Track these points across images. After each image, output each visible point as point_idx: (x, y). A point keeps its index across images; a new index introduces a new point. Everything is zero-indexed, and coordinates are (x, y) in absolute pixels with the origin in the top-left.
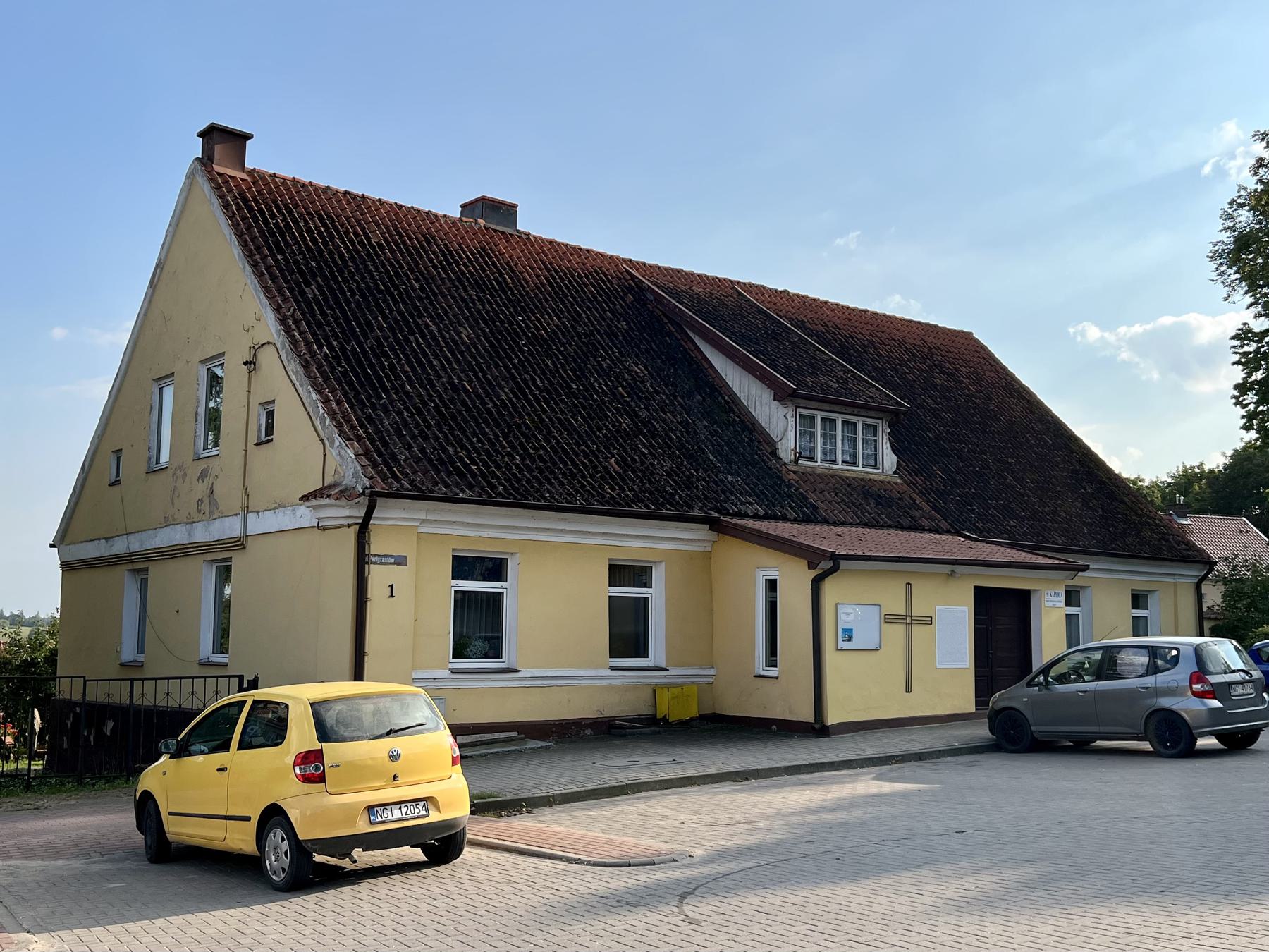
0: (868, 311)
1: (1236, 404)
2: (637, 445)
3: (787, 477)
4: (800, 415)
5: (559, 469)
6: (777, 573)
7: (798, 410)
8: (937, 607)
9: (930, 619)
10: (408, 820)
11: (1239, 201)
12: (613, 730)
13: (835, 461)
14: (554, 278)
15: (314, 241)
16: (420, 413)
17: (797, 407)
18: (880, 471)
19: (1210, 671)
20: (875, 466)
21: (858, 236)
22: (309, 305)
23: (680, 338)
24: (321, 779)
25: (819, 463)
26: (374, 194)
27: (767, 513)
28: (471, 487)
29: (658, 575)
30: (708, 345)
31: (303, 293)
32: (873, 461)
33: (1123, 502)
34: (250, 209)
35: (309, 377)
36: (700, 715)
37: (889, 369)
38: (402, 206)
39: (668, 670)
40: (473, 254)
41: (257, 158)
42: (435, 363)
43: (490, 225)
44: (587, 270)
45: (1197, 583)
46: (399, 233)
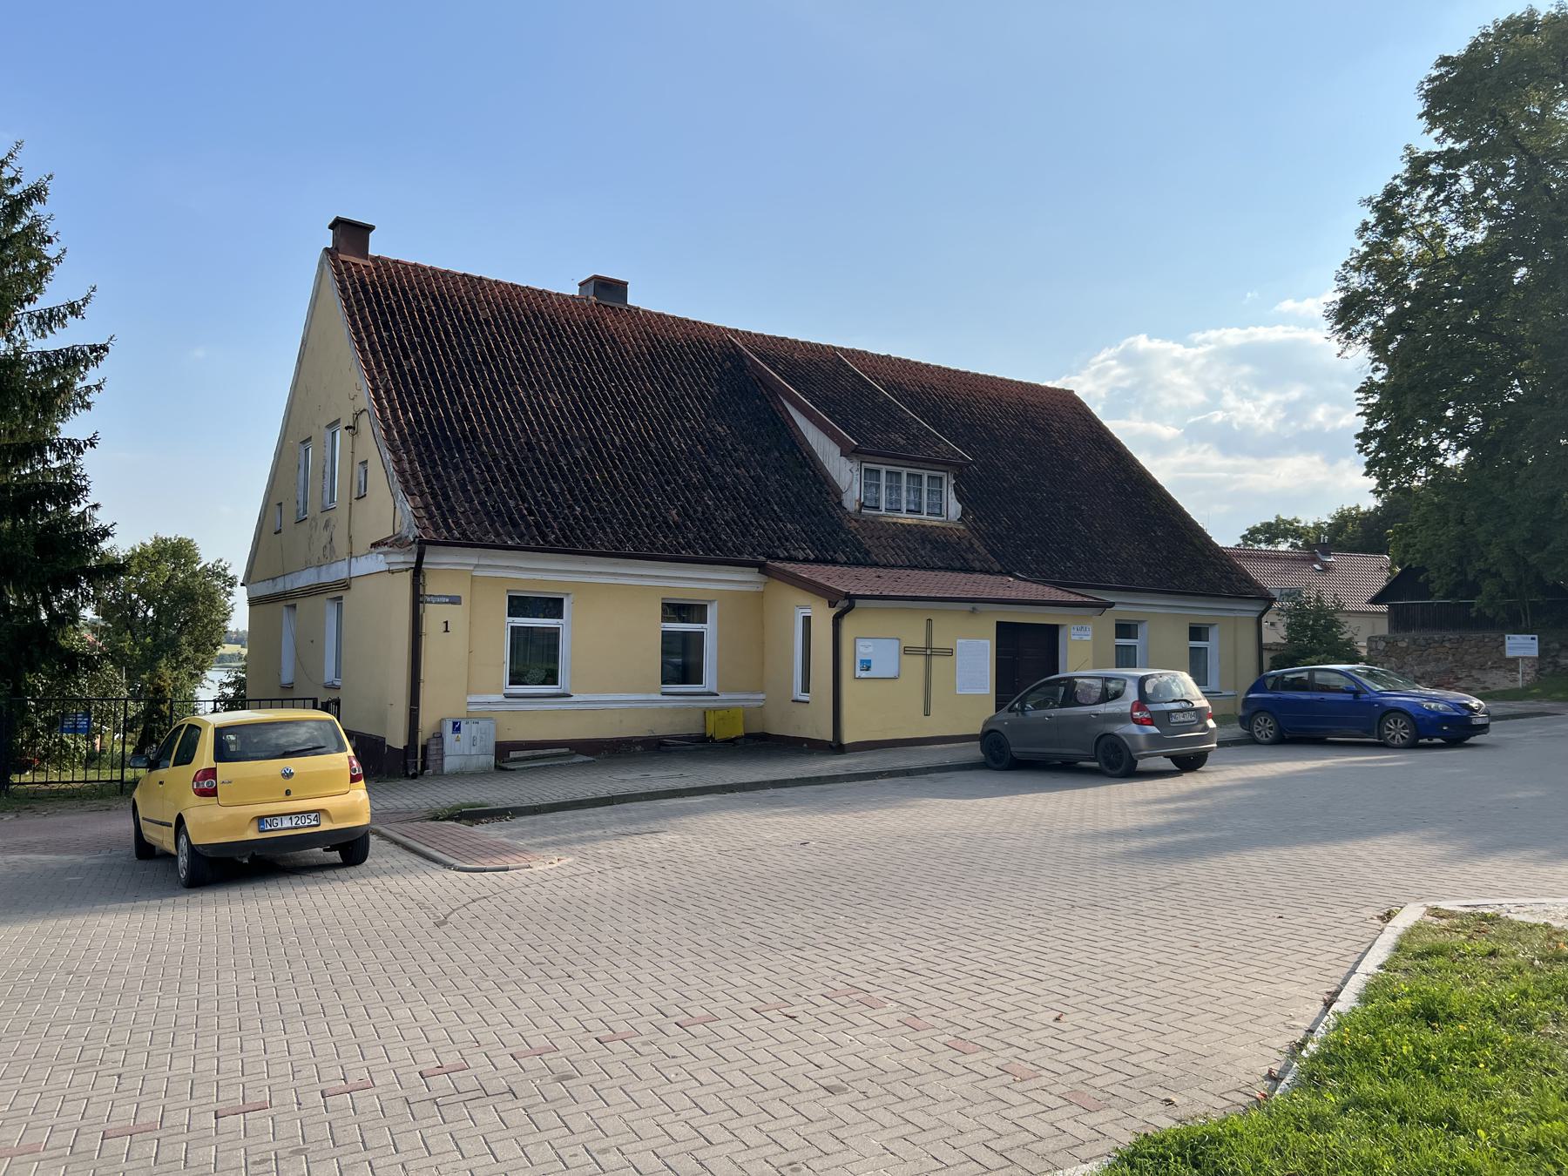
1: (1359, 452)
2: (702, 498)
5: (618, 519)
6: (809, 611)
11: (1352, 263)
14: (655, 348)
15: (423, 319)
16: (489, 469)
17: (861, 462)
20: (940, 515)
24: (212, 792)
25: (883, 512)
26: (491, 275)
27: (817, 557)
28: (521, 536)
29: (712, 612)
33: (1192, 544)
34: (366, 292)
38: (517, 286)
41: (377, 246)
46: (507, 310)
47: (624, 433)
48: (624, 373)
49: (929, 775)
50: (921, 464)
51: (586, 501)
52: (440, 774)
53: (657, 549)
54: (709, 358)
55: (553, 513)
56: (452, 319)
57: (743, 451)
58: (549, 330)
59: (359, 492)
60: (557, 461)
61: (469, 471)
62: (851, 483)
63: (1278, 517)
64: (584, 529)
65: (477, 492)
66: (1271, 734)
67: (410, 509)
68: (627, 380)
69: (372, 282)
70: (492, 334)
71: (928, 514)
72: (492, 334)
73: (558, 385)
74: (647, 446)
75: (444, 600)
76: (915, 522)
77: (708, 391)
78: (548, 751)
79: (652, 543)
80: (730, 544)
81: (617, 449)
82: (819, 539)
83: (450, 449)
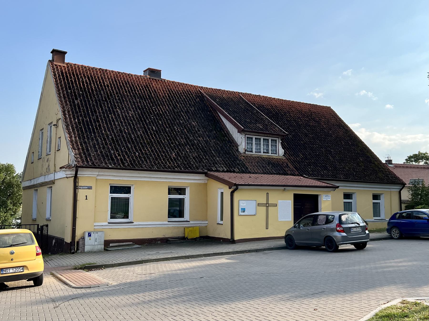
0: (290, 101)
2: (185, 149)
3: (240, 158)
4: (247, 137)
5: (152, 157)
6: (223, 190)
7: (246, 136)
9: (276, 205)
10: (15, 273)
12: (168, 242)
13: (260, 152)
15: (84, 85)
16: (105, 139)
17: (245, 135)
18: (278, 155)
19: (343, 223)
20: (276, 154)
21: (352, 71)
22: (75, 106)
23: (213, 112)
25: (254, 153)
27: (227, 170)
28: (115, 164)
29: (187, 191)
30: (222, 115)
31: (74, 102)
32: (275, 151)
33: (374, 163)
34: (63, 76)
35: (67, 129)
36: (200, 236)
37: (293, 120)
38: (120, 72)
39: (190, 222)
40: (142, 87)
41: (68, 59)
42: (116, 123)
43: (151, 77)
44: (184, 91)
45: (399, 191)
46: (116, 81)
47: (157, 126)
48: (158, 103)
49: (265, 252)
50: (268, 135)
51: (141, 150)
52: (83, 252)
53: (166, 168)
54: (191, 98)
55: (128, 155)
56: (94, 85)
57: (202, 131)
58: (131, 88)
59: (58, 148)
60: (131, 136)
61: (97, 140)
62: (242, 142)
63: (419, 152)
64: (139, 161)
65: (100, 148)
66: (398, 235)
67: (73, 155)
68: (159, 106)
69: (66, 72)
70: (109, 90)
71: (271, 153)
72: (109, 90)
73: (133, 108)
74: (165, 130)
75: (85, 188)
76: (267, 157)
77: (190, 109)
78: (124, 243)
79: (165, 166)
80: (194, 166)
81: (154, 131)
82: (228, 163)
83: (90, 133)
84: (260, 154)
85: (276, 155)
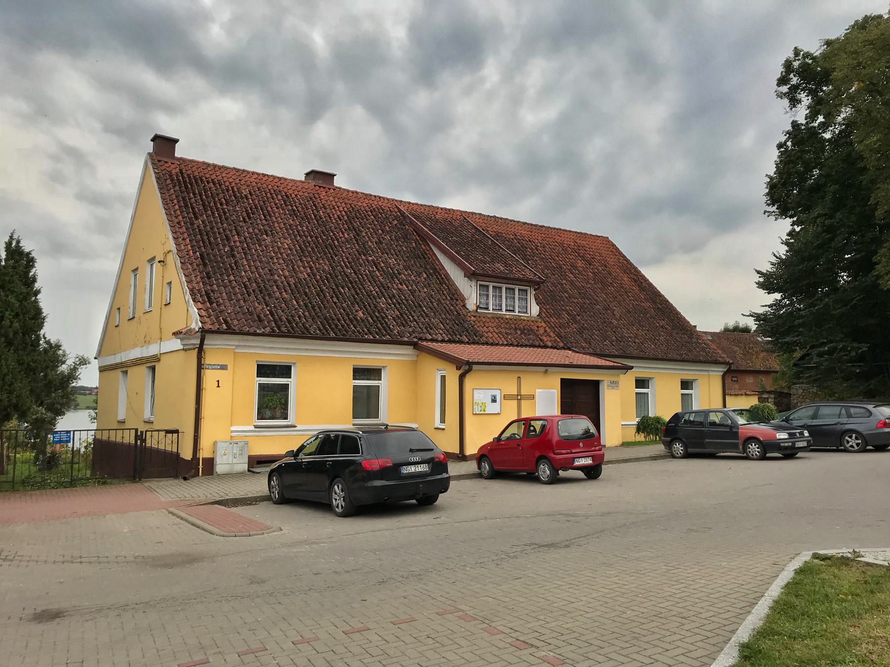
6: (445, 372)
7: (478, 282)
8: (537, 390)
20: (526, 312)
25: (491, 311)
41: (180, 152)
71: (519, 312)
75: (216, 367)
84: (513, 314)
85: (527, 315)
